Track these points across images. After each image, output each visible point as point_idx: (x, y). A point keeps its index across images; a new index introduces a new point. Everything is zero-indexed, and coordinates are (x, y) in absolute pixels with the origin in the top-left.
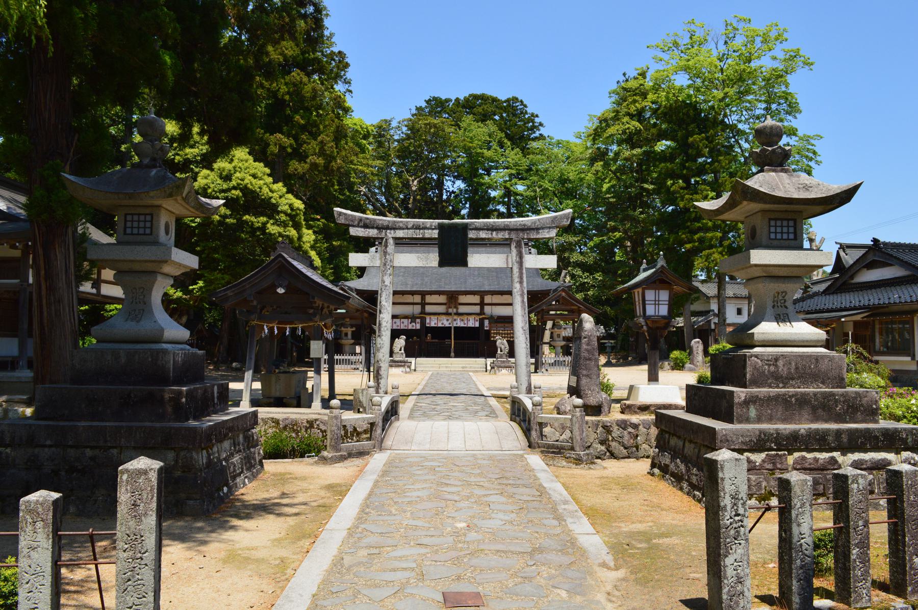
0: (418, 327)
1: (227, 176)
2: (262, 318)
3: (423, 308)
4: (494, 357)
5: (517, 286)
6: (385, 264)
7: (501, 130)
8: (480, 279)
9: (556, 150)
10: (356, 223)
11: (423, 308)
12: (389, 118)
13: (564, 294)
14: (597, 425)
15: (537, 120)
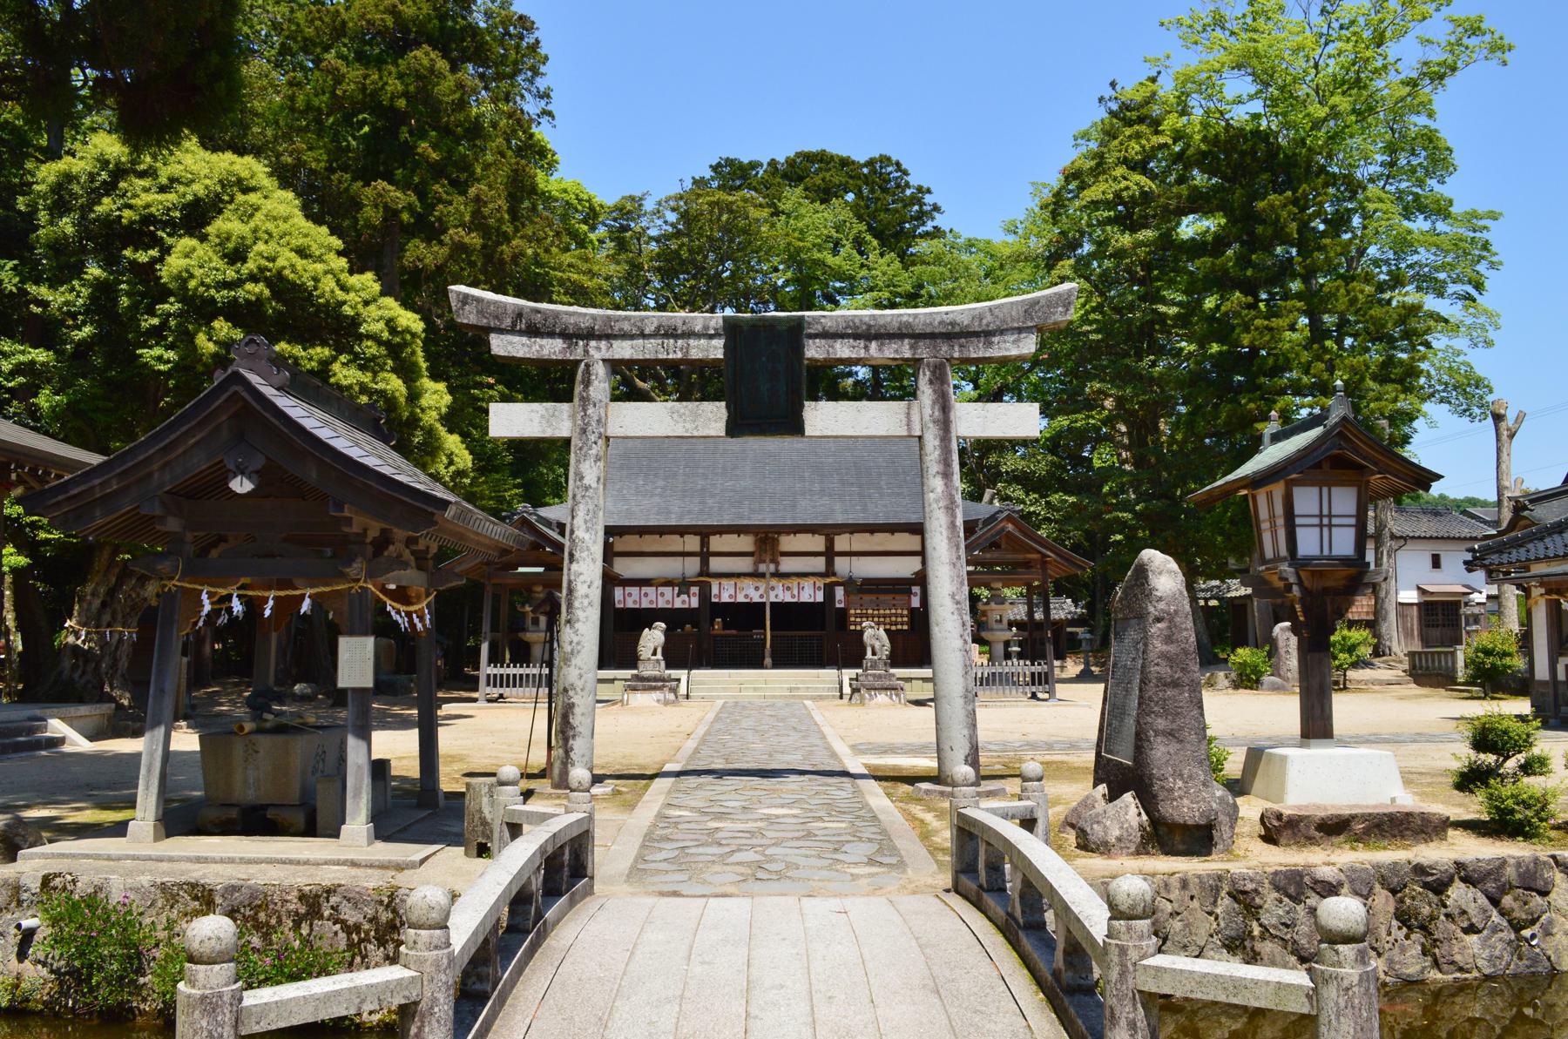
0: (695, 603)
1: (236, 250)
2: (199, 570)
3: (705, 563)
4: (859, 665)
5: (937, 484)
6: (584, 431)
7: (860, 218)
8: (826, 500)
9: (965, 257)
10: (508, 322)
11: (705, 563)
12: (638, 194)
13: (1010, 527)
14: (1216, 891)
15: (928, 199)
